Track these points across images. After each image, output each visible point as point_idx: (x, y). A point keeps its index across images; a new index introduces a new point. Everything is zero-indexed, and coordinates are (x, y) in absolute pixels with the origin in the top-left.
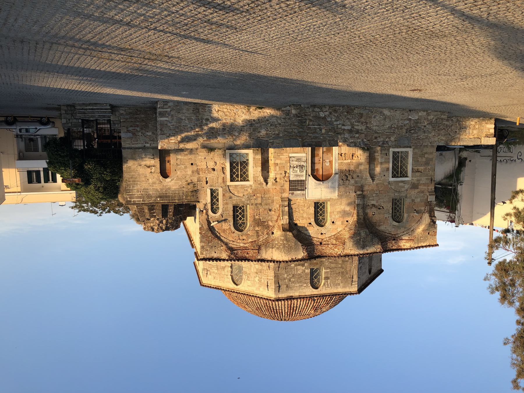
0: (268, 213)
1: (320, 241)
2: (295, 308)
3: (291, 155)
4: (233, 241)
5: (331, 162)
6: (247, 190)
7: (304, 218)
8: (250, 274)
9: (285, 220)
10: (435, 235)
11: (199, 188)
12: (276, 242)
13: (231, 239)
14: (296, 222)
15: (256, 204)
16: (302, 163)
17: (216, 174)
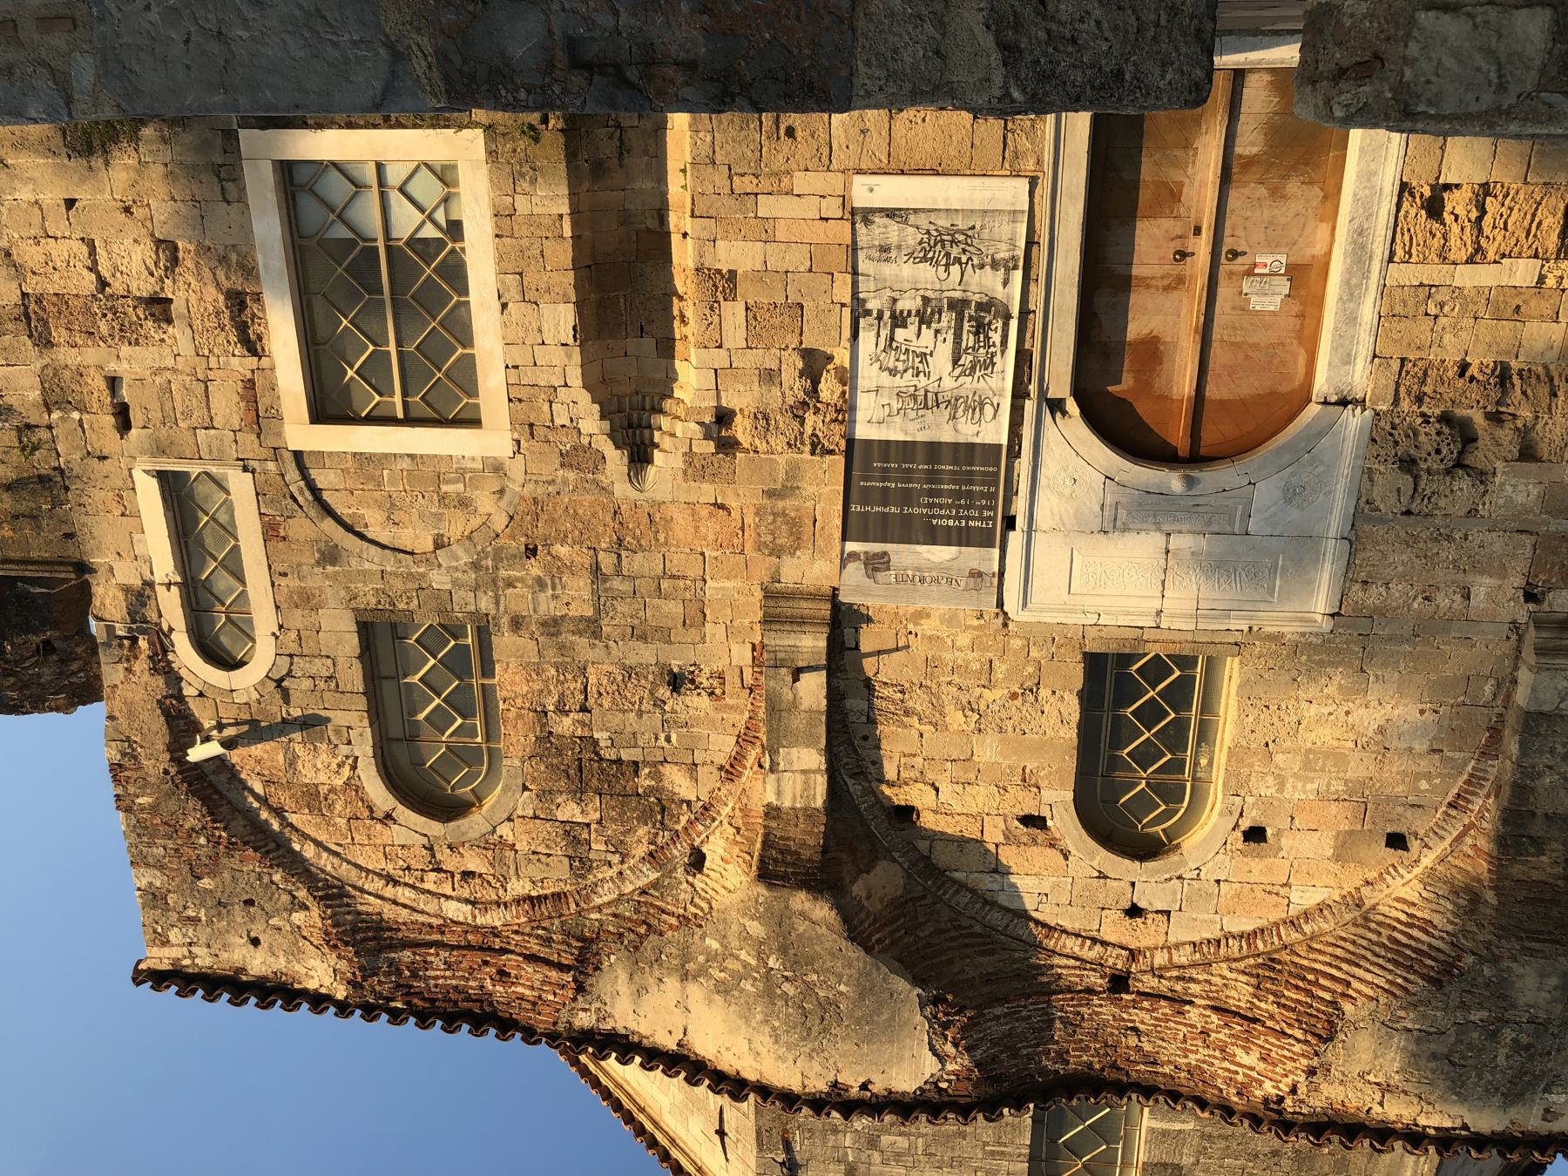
0: (659, 703)
3: (873, 191)
4: (391, 880)
5: (1305, 279)
6: (463, 503)
7: (981, 775)
9: (800, 778)
11: (68, 453)
13: (375, 862)
14: (899, 797)
15: (552, 626)
16: (986, 283)
17: (185, 346)
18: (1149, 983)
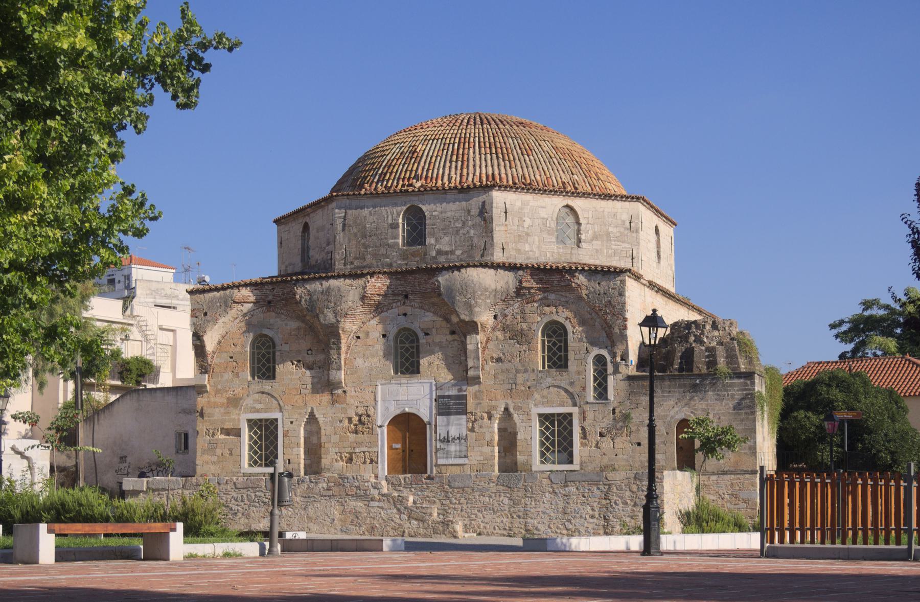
1: (408, 302)
2: (454, 158)
6: (543, 397)
8: (542, 231)
10: (193, 311)
12: (488, 301)
15: (526, 371)
18: (400, 298)
